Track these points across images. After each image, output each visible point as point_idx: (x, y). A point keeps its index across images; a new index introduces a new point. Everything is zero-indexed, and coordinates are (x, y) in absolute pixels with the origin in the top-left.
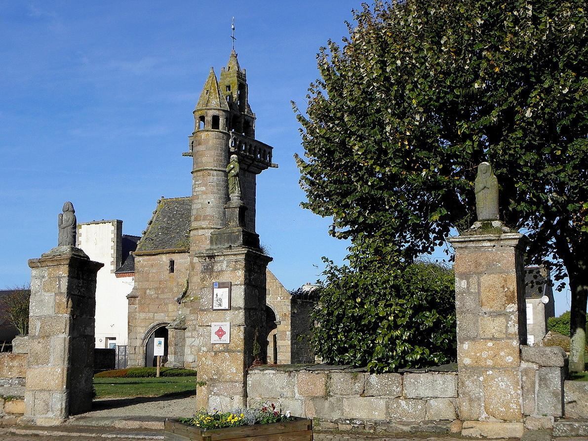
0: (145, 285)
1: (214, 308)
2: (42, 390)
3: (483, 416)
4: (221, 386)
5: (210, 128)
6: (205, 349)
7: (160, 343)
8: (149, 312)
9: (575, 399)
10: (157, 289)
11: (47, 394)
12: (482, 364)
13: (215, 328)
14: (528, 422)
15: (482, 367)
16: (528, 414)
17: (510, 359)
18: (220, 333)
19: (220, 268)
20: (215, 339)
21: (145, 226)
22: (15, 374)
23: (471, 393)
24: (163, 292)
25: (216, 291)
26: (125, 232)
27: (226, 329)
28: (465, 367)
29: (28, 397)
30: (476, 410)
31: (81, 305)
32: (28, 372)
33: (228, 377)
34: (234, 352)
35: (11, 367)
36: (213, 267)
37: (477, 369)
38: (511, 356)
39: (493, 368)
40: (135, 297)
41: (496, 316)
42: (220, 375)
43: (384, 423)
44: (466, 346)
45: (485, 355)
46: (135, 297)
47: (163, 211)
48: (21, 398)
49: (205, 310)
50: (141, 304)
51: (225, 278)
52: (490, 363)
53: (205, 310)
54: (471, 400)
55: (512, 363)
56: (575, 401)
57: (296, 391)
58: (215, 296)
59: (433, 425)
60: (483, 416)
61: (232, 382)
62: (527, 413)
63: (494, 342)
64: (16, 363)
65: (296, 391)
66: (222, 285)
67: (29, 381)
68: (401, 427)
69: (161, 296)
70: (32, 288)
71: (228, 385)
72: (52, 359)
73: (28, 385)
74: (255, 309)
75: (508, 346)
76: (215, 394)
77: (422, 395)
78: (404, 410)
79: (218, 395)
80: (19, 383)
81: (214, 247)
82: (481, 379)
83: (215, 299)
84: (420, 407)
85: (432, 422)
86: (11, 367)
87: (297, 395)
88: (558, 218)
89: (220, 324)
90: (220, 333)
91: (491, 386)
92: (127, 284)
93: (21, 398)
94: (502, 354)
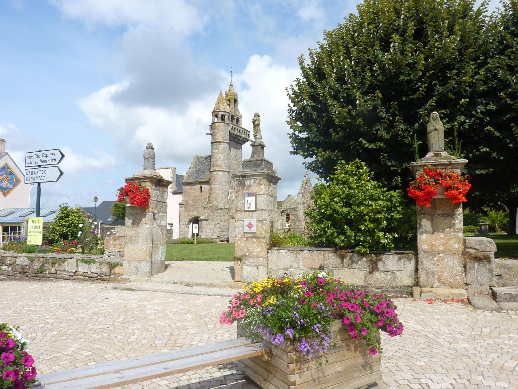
0: (188, 198)
1: (246, 209)
2: (133, 260)
3: (436, 284)
4: (251, 260)
5: (220, 121)
6: (239, 236)
7: (196, 227)
8: (190, 211)
9: (501, 274)
10: (193, 200)
11: (137, 263)
12: (436, 249)
13: (246, 223)
14: (469, 289)
15: (436, 251)
16: (470, 283)
17: (457, 246)
18: (250, 226)
19: (249, 184)
20: (246, 229)
21: (187, 170)
22: (117, 250)
23: (428, 269)
24: (196, 202)
25: (247, 198)
26: (177, 173)
27: (254, 222)
28: (424, 251)
29: (125, 264)
30: (431, 279)
31: (298, 123)
32: (125, 249)
33: (255, 254)
34: (259, 238)
35: (115, 245)
36: (244, 183)
37: (432, 253)
38: (458, 243)
39: (444, 252)
40: (183, 204)
41: (446, 217)
42: (250, 253)
43: (363, 287)
44: (424, 236)
45: (438, 242)
46: (183, 204)
47: (196, 162)
48: (121, 265)
49: (240, 211)
50: (185, 208)
51: (253, 190)
52: (442, 248)
53: (240, 211)
54: (427, 274)
55: (458, 248)
56: (500, 275)
57: (301, 264)
58: (246, 202)
59: (398, 289)
60: (436, 284)
61: (258, 257)
62: (469, 282)
63: (445, 234)
64: (117, 243)
65: (301, 264)
66: (251, 195)
67: (125, 254)
68: (375, 290)
69: (196, 204)
70: (224, 305)
71: (255, 259)
72: (140, 241)
73: (125, 256)
74: (271, 210)
75: (455, 237)
76: (247, 265)
77: (390, 269)
78: (377, 279)
79: (249, 266)
80: (120, 255)
81: (245, 170)
82: (435, 259)
83: (246, 204)
84: (389, 277)
85: (397, 287)
86: (115, 245)
87: (302, 267)
88: (488, 150)
89: (250, 219)
90: (250, 226)
91: (443, 264)
92: (179, 198)
93: (121, 265)
94: (451, 242)
